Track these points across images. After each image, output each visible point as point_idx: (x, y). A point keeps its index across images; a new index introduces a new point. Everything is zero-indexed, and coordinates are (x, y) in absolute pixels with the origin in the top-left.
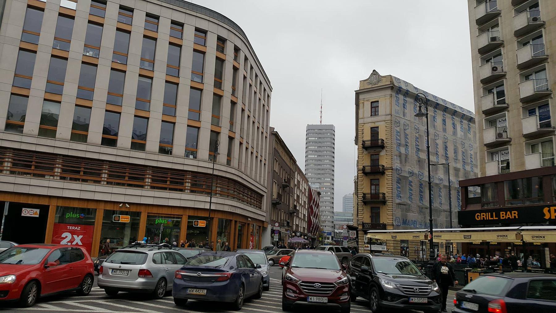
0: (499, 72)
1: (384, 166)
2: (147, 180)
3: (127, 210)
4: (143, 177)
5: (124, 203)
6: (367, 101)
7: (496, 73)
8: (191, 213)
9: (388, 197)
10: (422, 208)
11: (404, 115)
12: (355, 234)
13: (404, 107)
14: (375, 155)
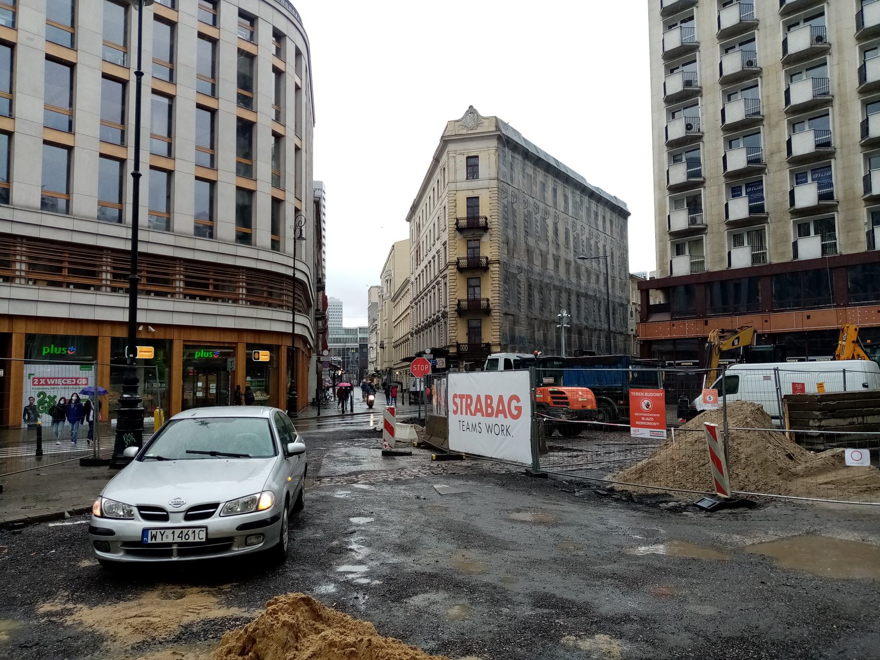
0: (693, 132)
2: (18, 266)
3: (150, 337)
6: (461, 154)
8: (250, 339)
9: (494, 305)
11: (512, 180)
12: (443, 364)
13: (511, 168)
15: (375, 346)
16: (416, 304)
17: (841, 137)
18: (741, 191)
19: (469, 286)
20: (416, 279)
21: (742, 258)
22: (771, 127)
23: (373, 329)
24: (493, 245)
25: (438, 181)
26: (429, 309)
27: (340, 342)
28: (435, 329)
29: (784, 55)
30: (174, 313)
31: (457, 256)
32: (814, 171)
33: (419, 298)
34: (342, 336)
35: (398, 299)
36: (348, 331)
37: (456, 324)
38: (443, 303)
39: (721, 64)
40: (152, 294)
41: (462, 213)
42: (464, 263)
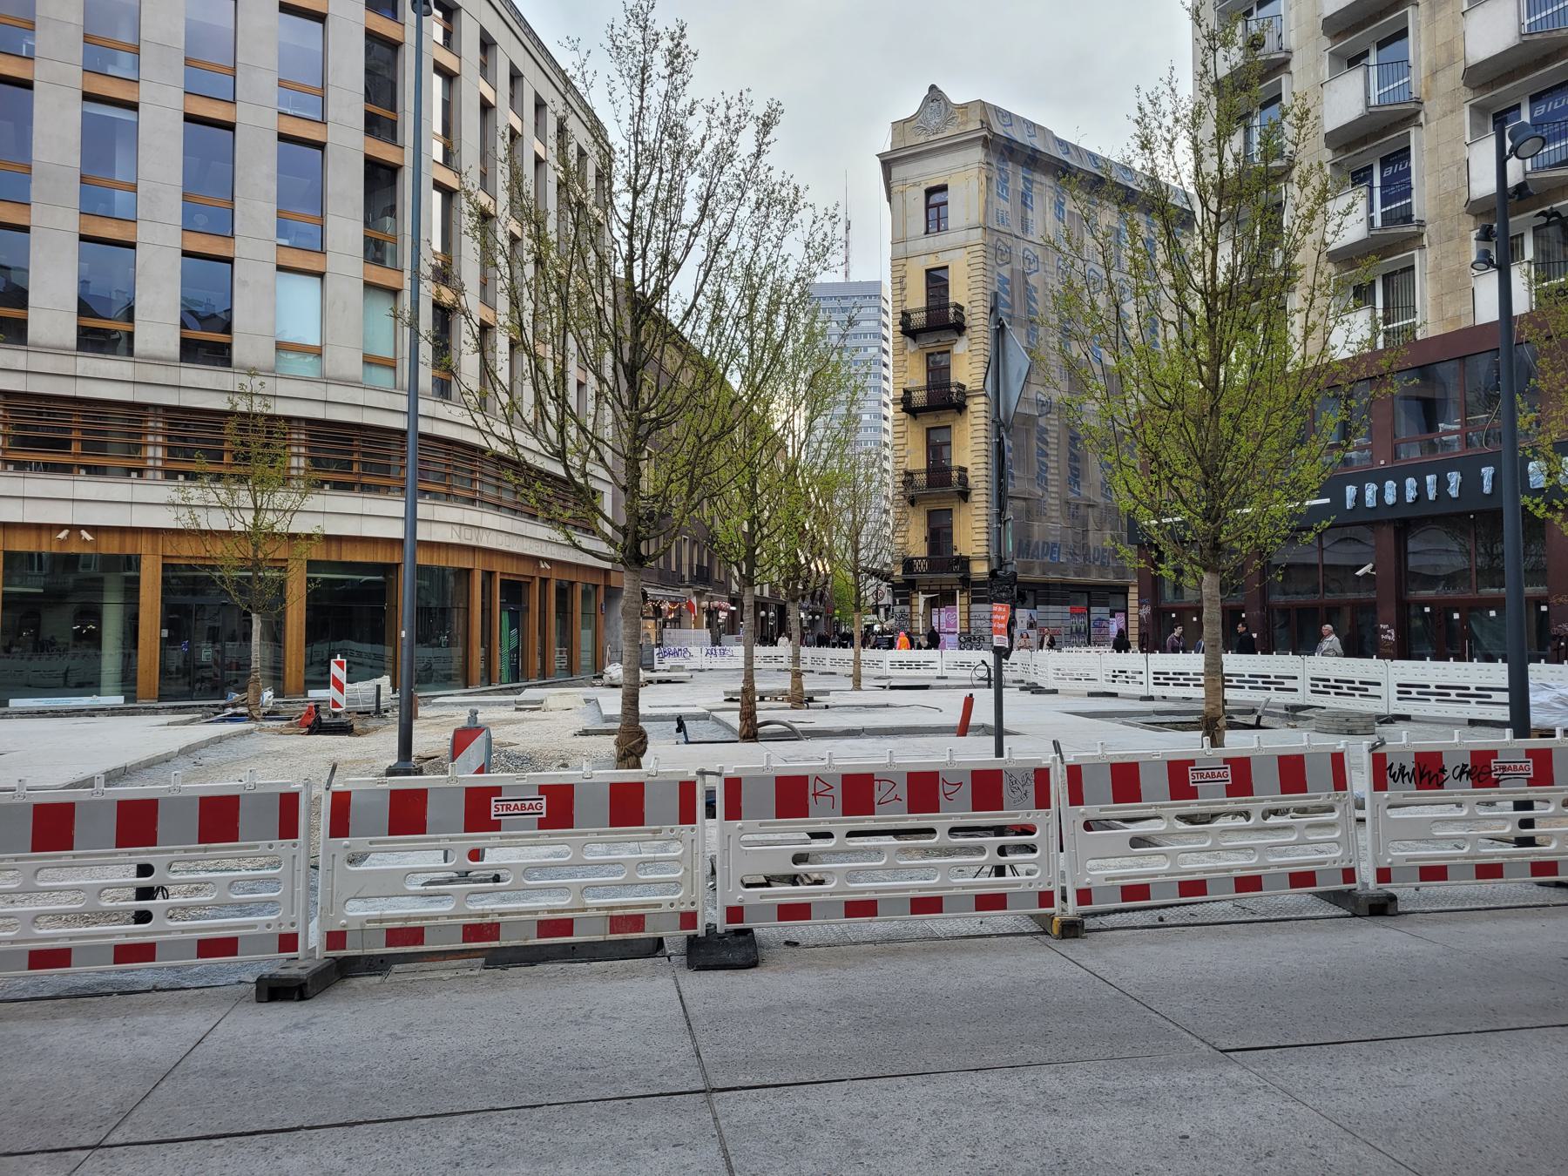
1: (963, 387)
2: (150, 452)
4: (102, 438)
5: (75, 529)
6: (914, 185)
7: (1262, 55)
10: (1077, 506)
11: (1025, 228)
13: (1024, 203)
14: (939, 353)
30: (134, 507)
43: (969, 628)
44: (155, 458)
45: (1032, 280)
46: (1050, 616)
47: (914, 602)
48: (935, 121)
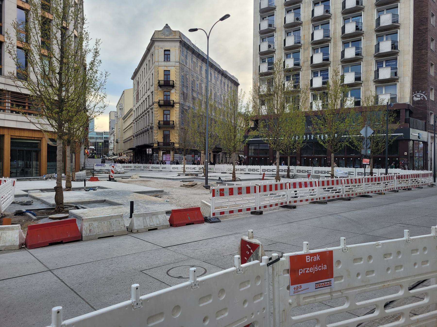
6: (161, 48)
11: (186, 64)
13: (186, 58)
15: (113, 141)
16: (136, 121)
17: (333, 57)
18: (383, 64)
19: (164, 114)
20: (136, 109)
21: (317, 106)
22: (305, 50)
23: (111, 133)
24: (177, 95)
25: (149, 61)
26: (142, 125)
27: (93, 139)
28: (146, 134)
29: (312, 17)
30: (5, 121)
31: (158, 99)
32: (321, 71)
33: (138, 119)
34: (95, 136)
35: (126, 119)
36: (98, 133)
37: (157, 132)
38: (151, 122)
39: (285, 18)
40: (14, 113)
41: (162, 77)
42: (162, 103)
43: (174, 160)
44: (8, 107)
45: (187, 76)
46: (189, 157)
47: (159, 153)
48: (167, 33)
